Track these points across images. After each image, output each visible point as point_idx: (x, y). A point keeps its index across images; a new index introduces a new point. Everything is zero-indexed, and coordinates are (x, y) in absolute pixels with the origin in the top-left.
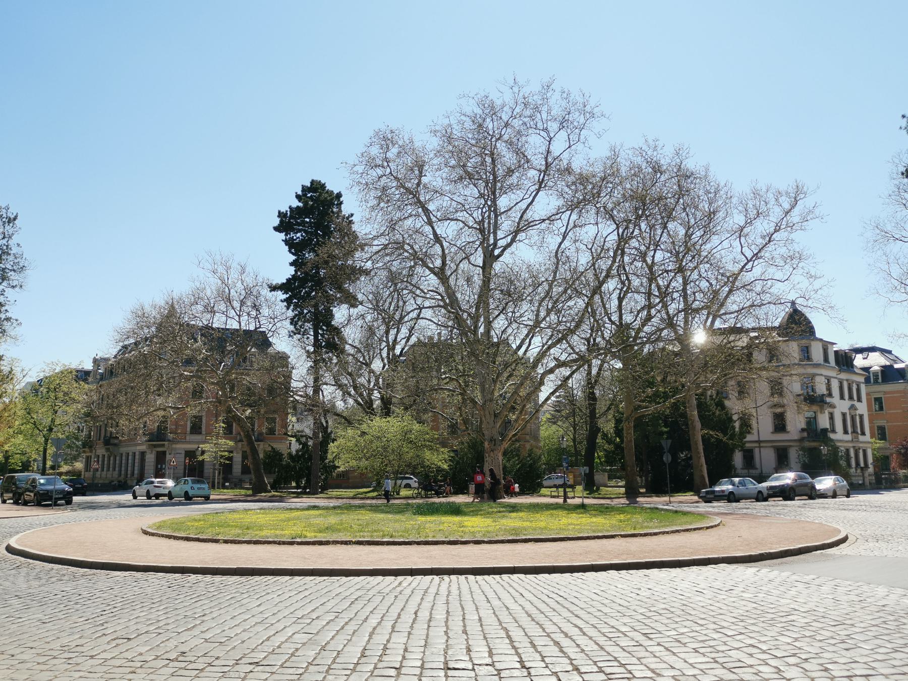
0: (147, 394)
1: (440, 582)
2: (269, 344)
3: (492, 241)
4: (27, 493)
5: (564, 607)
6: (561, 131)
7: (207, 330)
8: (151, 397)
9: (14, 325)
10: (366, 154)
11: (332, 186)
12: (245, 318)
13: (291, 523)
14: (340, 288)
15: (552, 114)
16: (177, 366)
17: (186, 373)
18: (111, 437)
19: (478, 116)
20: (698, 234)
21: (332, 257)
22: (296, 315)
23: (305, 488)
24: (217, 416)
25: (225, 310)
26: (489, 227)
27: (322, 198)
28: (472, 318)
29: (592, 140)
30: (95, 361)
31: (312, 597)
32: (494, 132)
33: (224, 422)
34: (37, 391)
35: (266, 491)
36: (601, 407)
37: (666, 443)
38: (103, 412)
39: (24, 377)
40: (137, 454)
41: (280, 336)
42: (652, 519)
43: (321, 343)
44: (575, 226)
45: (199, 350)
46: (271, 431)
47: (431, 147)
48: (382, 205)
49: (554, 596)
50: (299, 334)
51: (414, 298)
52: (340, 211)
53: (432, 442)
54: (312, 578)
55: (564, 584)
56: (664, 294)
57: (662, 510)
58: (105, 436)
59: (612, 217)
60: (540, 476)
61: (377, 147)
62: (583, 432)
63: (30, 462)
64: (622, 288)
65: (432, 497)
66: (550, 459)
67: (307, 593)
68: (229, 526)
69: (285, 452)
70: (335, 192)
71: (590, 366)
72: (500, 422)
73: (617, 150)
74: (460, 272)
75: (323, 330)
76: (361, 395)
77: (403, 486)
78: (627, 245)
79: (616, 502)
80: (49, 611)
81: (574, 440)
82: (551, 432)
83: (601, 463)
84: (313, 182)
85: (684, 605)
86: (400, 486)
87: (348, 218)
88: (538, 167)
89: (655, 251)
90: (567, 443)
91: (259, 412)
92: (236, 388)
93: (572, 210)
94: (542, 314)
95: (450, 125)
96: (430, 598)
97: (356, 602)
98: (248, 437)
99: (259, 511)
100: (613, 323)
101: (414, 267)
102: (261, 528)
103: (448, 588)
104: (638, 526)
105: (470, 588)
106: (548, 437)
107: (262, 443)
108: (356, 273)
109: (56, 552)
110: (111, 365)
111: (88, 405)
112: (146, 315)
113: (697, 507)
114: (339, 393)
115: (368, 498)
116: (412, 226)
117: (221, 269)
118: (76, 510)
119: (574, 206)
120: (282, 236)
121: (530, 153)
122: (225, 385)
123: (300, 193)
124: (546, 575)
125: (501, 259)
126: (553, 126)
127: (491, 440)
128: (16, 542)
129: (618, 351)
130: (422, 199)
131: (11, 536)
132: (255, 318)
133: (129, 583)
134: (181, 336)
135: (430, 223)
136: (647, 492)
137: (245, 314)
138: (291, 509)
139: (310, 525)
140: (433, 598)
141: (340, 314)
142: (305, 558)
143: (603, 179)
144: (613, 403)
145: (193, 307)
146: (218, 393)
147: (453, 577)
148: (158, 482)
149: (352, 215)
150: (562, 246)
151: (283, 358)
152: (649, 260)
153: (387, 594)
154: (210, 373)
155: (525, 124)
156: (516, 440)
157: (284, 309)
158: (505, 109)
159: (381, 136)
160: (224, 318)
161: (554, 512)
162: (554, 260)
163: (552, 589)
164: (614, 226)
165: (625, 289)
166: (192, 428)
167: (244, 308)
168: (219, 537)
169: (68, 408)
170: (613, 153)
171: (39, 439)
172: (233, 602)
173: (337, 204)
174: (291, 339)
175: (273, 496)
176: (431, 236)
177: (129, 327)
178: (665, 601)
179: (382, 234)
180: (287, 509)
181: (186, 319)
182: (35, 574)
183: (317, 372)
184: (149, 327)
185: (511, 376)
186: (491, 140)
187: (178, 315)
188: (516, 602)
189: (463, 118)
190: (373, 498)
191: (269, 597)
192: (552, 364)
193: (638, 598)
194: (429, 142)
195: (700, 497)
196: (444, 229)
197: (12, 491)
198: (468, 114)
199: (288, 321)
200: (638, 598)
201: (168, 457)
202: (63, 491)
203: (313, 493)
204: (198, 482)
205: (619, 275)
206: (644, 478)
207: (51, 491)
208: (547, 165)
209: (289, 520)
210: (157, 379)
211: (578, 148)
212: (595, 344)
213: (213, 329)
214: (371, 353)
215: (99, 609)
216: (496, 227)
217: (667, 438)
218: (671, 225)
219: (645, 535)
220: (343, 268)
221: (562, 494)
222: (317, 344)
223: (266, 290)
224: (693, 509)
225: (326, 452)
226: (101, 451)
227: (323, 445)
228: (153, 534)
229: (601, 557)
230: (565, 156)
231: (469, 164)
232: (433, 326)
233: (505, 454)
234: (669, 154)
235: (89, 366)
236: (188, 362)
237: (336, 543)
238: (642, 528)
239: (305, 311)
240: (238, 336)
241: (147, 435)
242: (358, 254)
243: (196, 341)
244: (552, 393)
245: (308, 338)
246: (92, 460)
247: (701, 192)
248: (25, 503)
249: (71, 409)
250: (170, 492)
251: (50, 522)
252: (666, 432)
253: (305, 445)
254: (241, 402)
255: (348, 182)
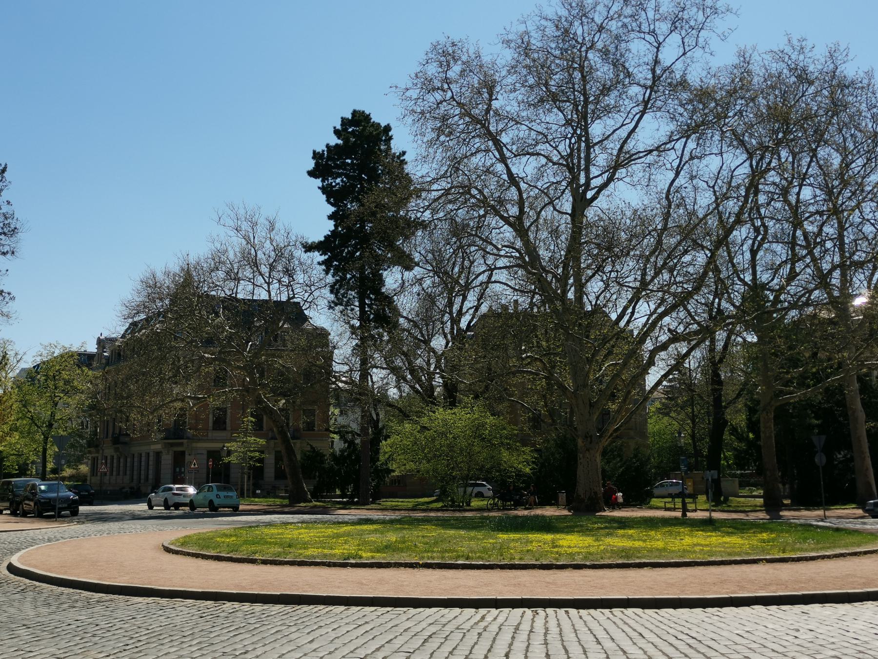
0: (162, 381)
1: (534, 617)
2: (305, 319)
3: (582, 181)
4: (27, 502)
5: (699, 652)
6: (673, 33)
7: (231, 302)
8: (166, 385)
9: (7, 299)
10: (421, 74)
11: (379, 117)
12: (275, 286)
13: (342, 539)
14: (391, 246)
15: (661, 11)
16: (196, 347)
17: (206, 355)
18: (120, 434)
19: (563, 19)
20: (860, 162)
21: (381, 207)
22: (337, 281)
23: (352, 497)
24: (244, 408)
25: (251, 276)
26: (579, 162)
27: (367, 133)
28: (558, 280)
29: (715, 43)
30: (100, 342)
31: (375, 632)
32: (584, 39)
33: (252, 415)
34: (33, 379)
35: (306, 501)
36: (729, 392)
37: (819, 441)
38: (111, 403)
39: (18, 362)
40: (151, 454)
41: (319, 307)
42: (805, 539)
43: (369, 315)
44: (692, 158)
45: (221, 327)
46: (310, 426)
47: (503, 62)
48: (442, 138)
49: (684, 637)
50: (341, 305)
51: (483, 257)
52: (389, 148)
53: (510, 439)
54: (373, 608)
55: (695, 621)
56: (811, 243)
57: (818, 527)
58: (113, 433)
59: (742, 143)
60: (650, 483)
61: (435, 64)
62: (705, 426)
63: (27, 465)
64: (756, 237)
65: (511, 509)
66: (662, 461)
67: (368, 627)
68: (266, 543)
69: (327, 452)
70: (383, 125)
71: (713, 341)
72: (597, 414)
73: (747, 55)
74: (541, 221)
75: (371, 299)
76: (419, 381)
77: (473, 495)
78: (763, 180)
79: (752, 516)
80: (63, 644)
81: (693, 436)
82: (662, 426)
83: (729, 466)
84: (355, 113)
85: (860, 652)
86: (471, 495)
87: (399, 157)
88: (642, 82)
89: (801, 186)
90: (684, 439)
91: (294, 402)
92: (266, 373)
93: (688, 137)
94: (650, 273)
95: (527, 33)
96: (522, 636)
97: (430, 640)
98: (283, 433)
99: (300, 525)
100: (745, 283)
101: (484, 216)
102: (305, 545)
103: (545, 625)
104: (788, 548)
105: (573, 625)
106: (659, 433)
107: (298, 441)
108: (413, 226)
109: (65, 573)
110: (119, 346)
111: (94, 395)
112: (158, 285)
113: (865, 523)
114: (392, 378)
115: (432, 510)
116: (480, 164)
117: (245, 226)
118: (83, 523)
119: (686, 133)
120: (318, 182)
121: (633, 63)
122: (253, 369)
123: (339, 127)
124: (671, 611)
125: (594, 204)
126: (663, 28)
127: (586, 437)
128: (19, 560)
129: (753, 319)
130: (492, 129)
131: (12, 553)
132: (287, 286)
133: (153, 611)
134: (200, 310)
135: (503, 160)
136: (792, 504)
137: (275, 281)
138: (339, 523)
139: (365, 543)
140: (526, 637)
141: (392, 278)
142: (362, 584)
143: (731, 93)
144: (745, 389)
145: (213, 274)
146: (244, 380)
147: (550, 611)
148: (178, 489)
149: (404, 153)
150: (676, 184)
151: (322, 335)
152: (792, 199)
153: (469, 631)
154: (235, 355)
155: (624, 26)
156: (617, 437)
157: (322, 276)
158: (598, 8)
159: (440, 51)
160: (250, 287)
161: (676, 529)
162: (664, 202)
163: (680, 628)
164: (745, 156)
165: (759, 238)
166: (215, 423)
167: (274, 273)
168: (257, 557)
169: (70, 400)
170: (742, 59)
171: (37, 437)
172: (279, 637)
173: (385, 140)
174: (331, 311)
175: (315, 506)
176: (505, 177)
177: (139, 299)
178: (833, 646)
179: (443, 176)
180: (334, 523)
181: (206, 289)
182: (42, 599)
183: (364, 352)
184: (161, 299)
185: (610, 353)
186: (580, 51)
187: (195, 284)
188: (635, 644)
189: (543, 22)
190: (437, 510)
191: (323, 631)
192: (664, 338)
193: (797, 641)
194: (501, 56)
195: (865, 511)
196: (522, 167)
197: (8, 500)
198: (550, 17)
199: (328, 288)
200: (797, 641)
201: (188, 458)
202: (67, 499)
203: (363, 503)
204: (225, 489)
205: (752, 220)
206: (787, 486)
207: (54, 499)
208: (656, 79)
209: (338, 536)
210: (173, 363)
211: (695, 55)
212: (720, 311)
213: (238, 300)
214: (430, 327)
215: (121, 642)
216: (588, 161)
217: (819, 434)
218: (822, 153)
219: (799, 560)
220: (395, 220)
221: (679, 505)
222: (363, 317)
223: (300, 251)
224: (858, 527)
225: (377, 452)
226: (109, 451)
227: (374, 444)
228: (177, 552)
229: (742, 588)
230: (679, 65)
231: (552, 83)
232: (509, 291)
233: (604, 453)
234: (821, 57)
235: (92, 348)
236: (209, 342)
237: (398, 565)
238: (793, 550)
239: (348, 276)
240: (268, 308)
241: (163, 431)
242: (412, 203)
243: (217, 315)
244: (665, 376)
245: (352, 310)
246: (99, 462)
247: (863, 107)
248: (25, 514)
249: (73, 401)
250: (191, 501)
251: (55, 537)
252: (817, 426)
253: (351, 443)
254: (273, 390)
255: (399, 112)
